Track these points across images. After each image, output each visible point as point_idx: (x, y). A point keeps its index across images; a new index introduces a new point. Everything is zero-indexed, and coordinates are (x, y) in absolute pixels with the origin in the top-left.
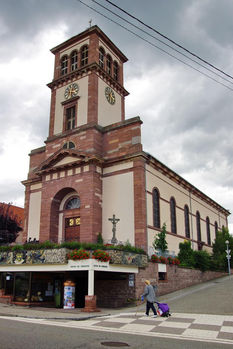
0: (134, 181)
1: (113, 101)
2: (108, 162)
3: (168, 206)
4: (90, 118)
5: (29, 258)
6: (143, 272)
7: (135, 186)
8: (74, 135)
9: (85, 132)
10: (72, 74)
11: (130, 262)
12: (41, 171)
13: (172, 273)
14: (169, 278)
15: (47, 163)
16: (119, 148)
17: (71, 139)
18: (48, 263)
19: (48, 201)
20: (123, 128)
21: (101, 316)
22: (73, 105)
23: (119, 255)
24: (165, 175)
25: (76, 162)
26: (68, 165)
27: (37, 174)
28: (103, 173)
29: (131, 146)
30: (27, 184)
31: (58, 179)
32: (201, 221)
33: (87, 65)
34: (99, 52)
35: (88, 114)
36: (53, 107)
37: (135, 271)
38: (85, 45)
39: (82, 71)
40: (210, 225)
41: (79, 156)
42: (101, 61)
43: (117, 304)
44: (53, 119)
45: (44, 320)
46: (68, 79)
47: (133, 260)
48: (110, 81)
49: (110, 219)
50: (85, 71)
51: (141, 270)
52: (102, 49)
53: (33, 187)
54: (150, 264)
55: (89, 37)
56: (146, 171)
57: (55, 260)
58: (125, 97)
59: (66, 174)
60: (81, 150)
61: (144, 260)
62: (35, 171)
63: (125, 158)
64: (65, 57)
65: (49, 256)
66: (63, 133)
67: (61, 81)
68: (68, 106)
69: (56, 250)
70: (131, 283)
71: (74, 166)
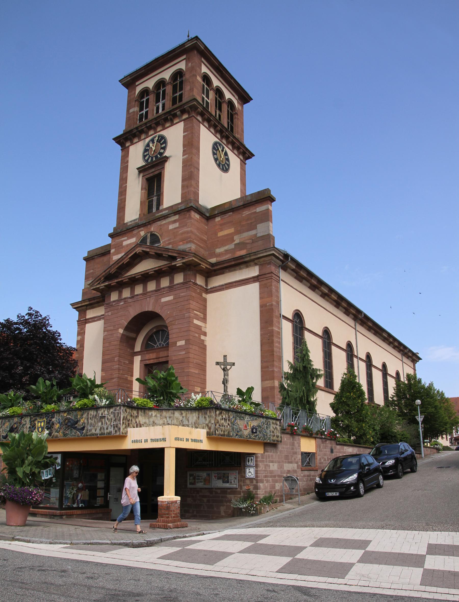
0: (261, 298)
1: (226, 165)
2: (215, 268)
3: (319, 342)
4: (186, 192)
5: (57, 426)
6: (271, 453)
7: (261, 306)
8: (158, 222)
9: (177, 217)
10: (156, 119)
11: (246, 432)
12: (102, 285)
13: (325, 455)
14: (320, 463)
15: (113, 270)
16: (236, 242)
17: (153, 228)
18: (91, 435)
19: (115, 335)
20: (242, 208)
21: (186, 537)
22: (157, 173)
23: (225, 420)
24: (314, 290)
25: (162, 267)
26: (148, 273)
27: (97, 289)
28: (207, 287)
29: (255, 239)
30: (80, 309)
31: (132, 297)
32: (374, 370)
33: (181, 103)
34: (202, 83)
35: (183, 187)
36: (124, 177)
37: (259, 450)
38: (179, 70)
39: (172, 113)
40: (388, 377)
41: (167, 256)
42: (206, 98)
43: (224, 511)
44: (123, 197)
45: (64, 548)
46: (150, 128)
47: (252, 430)
48: (221, 132)
49: (217, 363)
50: (178, 113)
51: (269, 449)
52: (206, 78)
53: (90, 314)
54: (286, 438)
55: (184, 57)
56: (281, 282)
57: (104, 428)
58: (247, 162)
59: (145, 288)
60: (170, 247)
61: (273, 430)
62: (93, 284)
63: (246, 259)
64: (145, 92)
65: (93, 422)
66: (140, 218)
67: (138, 133)
68: (149, 174)
69: (104, 411)
70: (250, 473)
71: (157, 275)
